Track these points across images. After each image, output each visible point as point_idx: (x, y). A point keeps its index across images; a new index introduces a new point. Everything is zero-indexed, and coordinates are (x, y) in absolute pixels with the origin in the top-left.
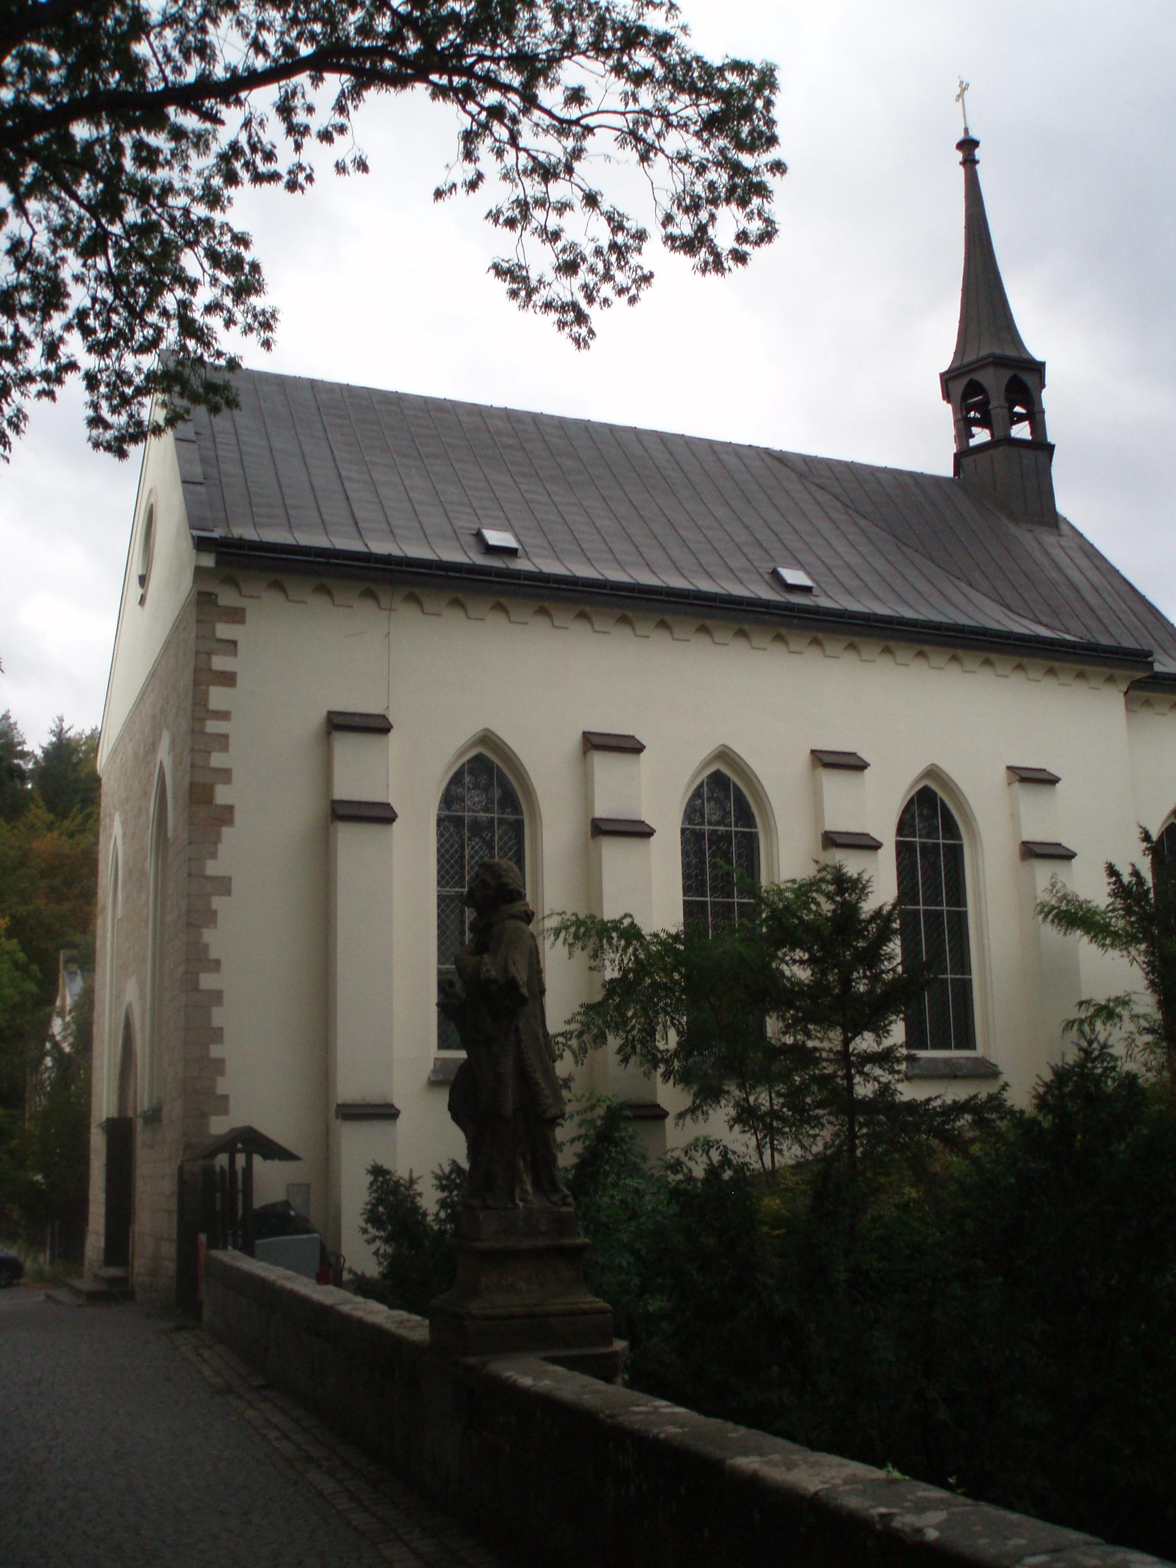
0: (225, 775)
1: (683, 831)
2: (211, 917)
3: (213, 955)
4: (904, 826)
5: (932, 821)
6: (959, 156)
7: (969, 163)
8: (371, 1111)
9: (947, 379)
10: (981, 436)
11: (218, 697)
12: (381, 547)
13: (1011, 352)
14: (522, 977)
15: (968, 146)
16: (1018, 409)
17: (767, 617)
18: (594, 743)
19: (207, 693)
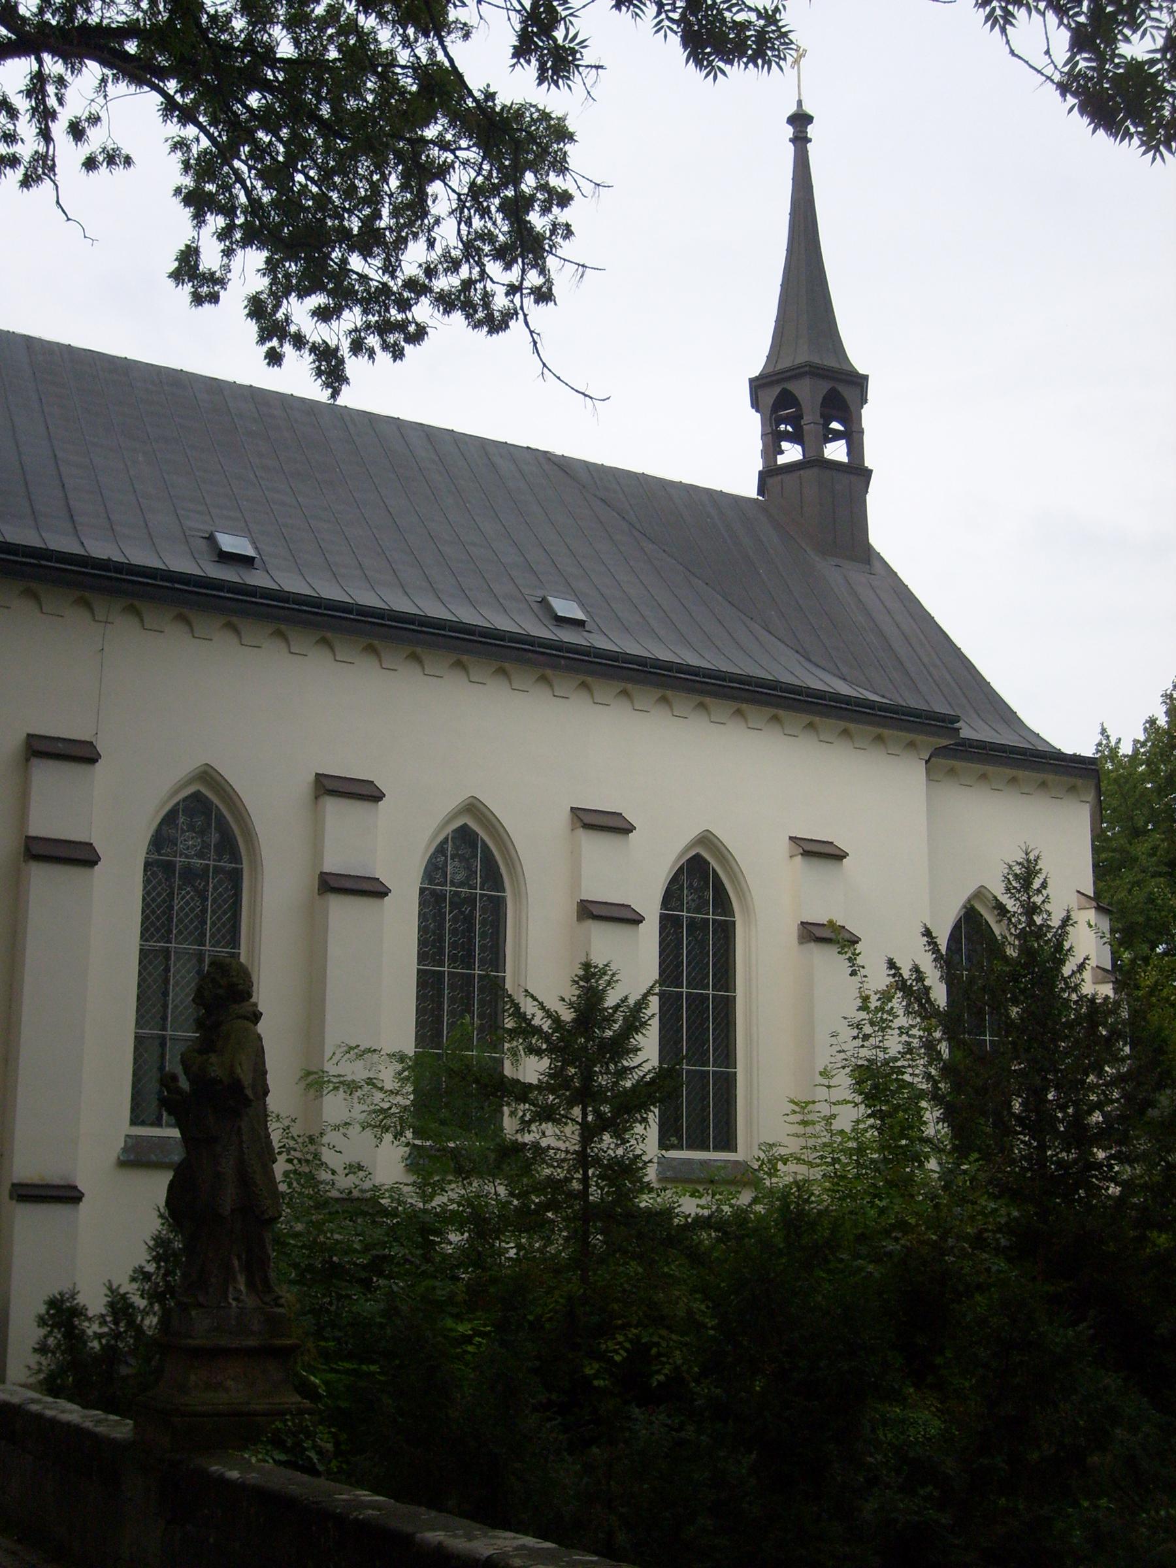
1: (422, 891)
4: (670, 897)
5: (701, 902)
6: (789, 131)
7: (800, 141)
9: (758, 386)
10: (791, 453)
12: (100, 549)
13: (830, 362)
14: (247, 1079)
15: (800, 120)
16: (835, 425)
17: (530, 655)
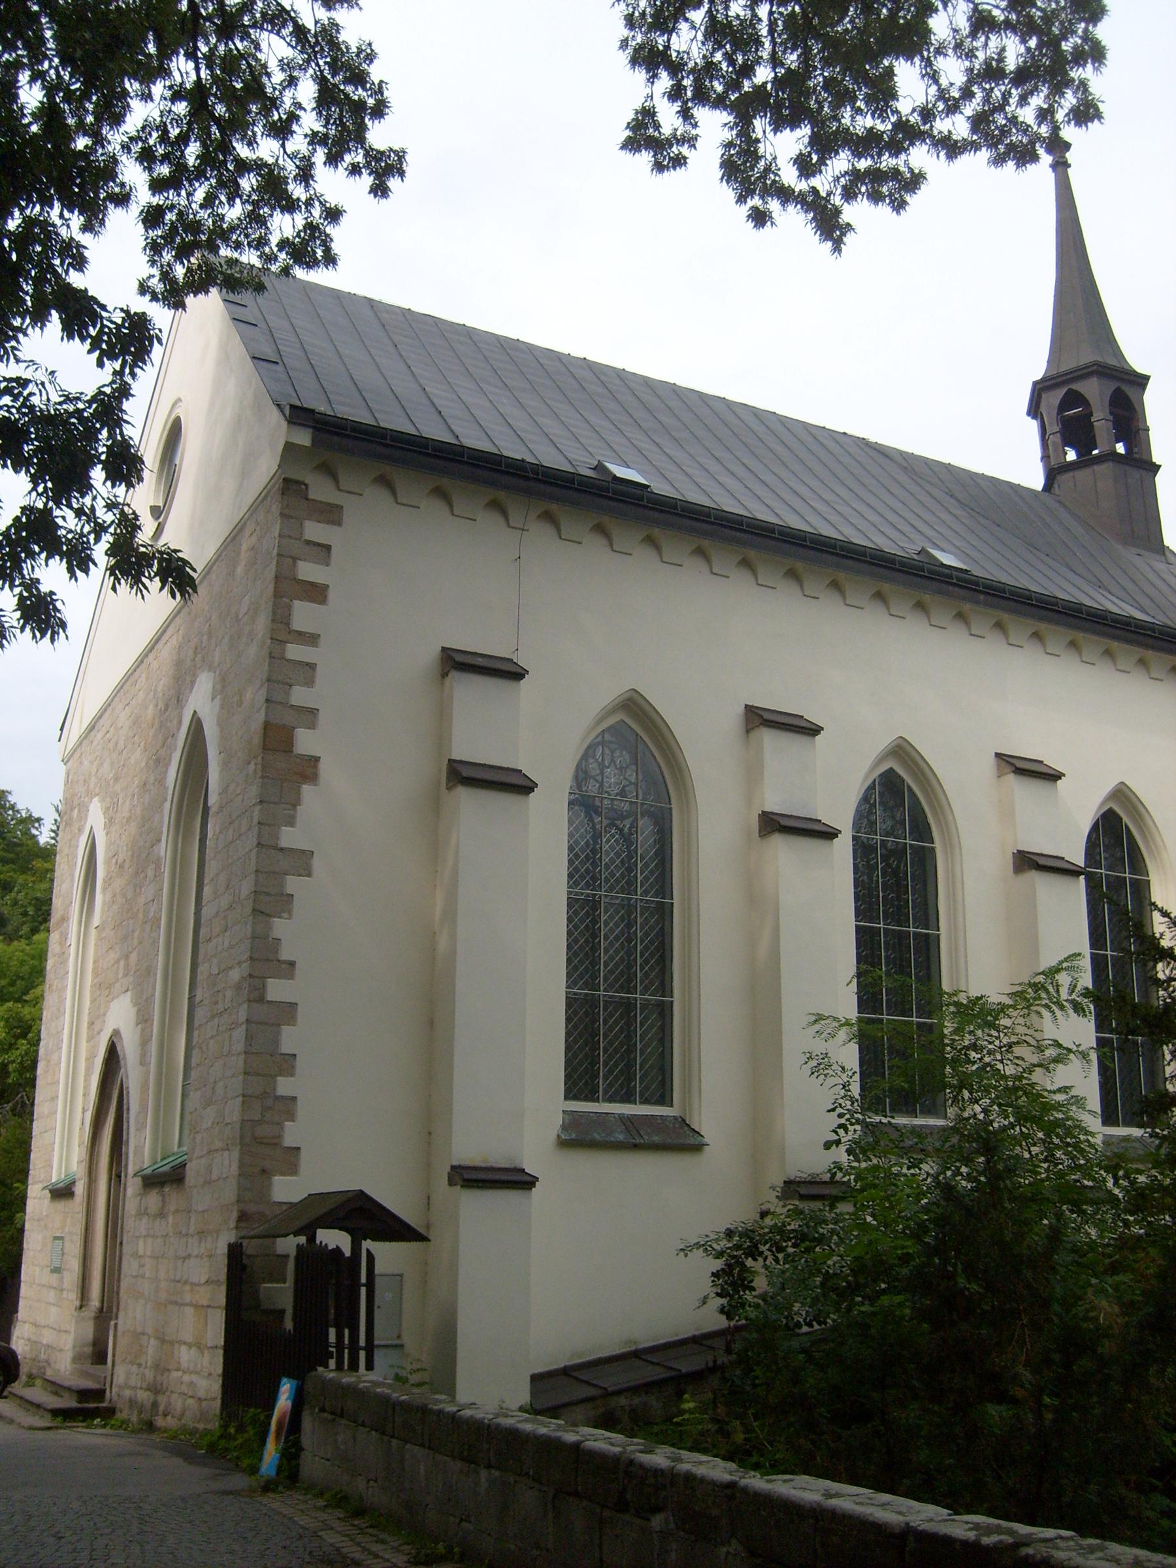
0: (310, 715)
2: (284, 903)
3: (285, 954)
8: (490, 1176)
11: (303, 615)
18: (758, 719)
19: (289, 607)
